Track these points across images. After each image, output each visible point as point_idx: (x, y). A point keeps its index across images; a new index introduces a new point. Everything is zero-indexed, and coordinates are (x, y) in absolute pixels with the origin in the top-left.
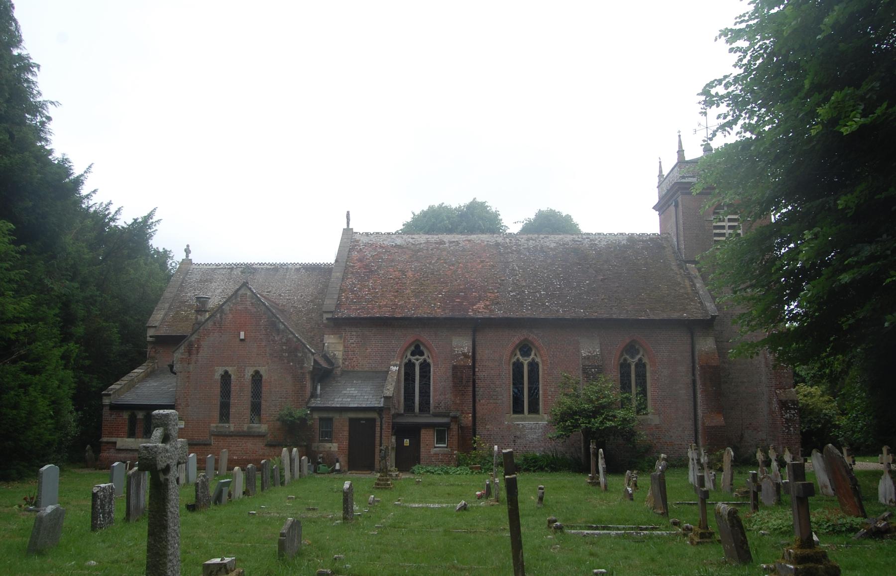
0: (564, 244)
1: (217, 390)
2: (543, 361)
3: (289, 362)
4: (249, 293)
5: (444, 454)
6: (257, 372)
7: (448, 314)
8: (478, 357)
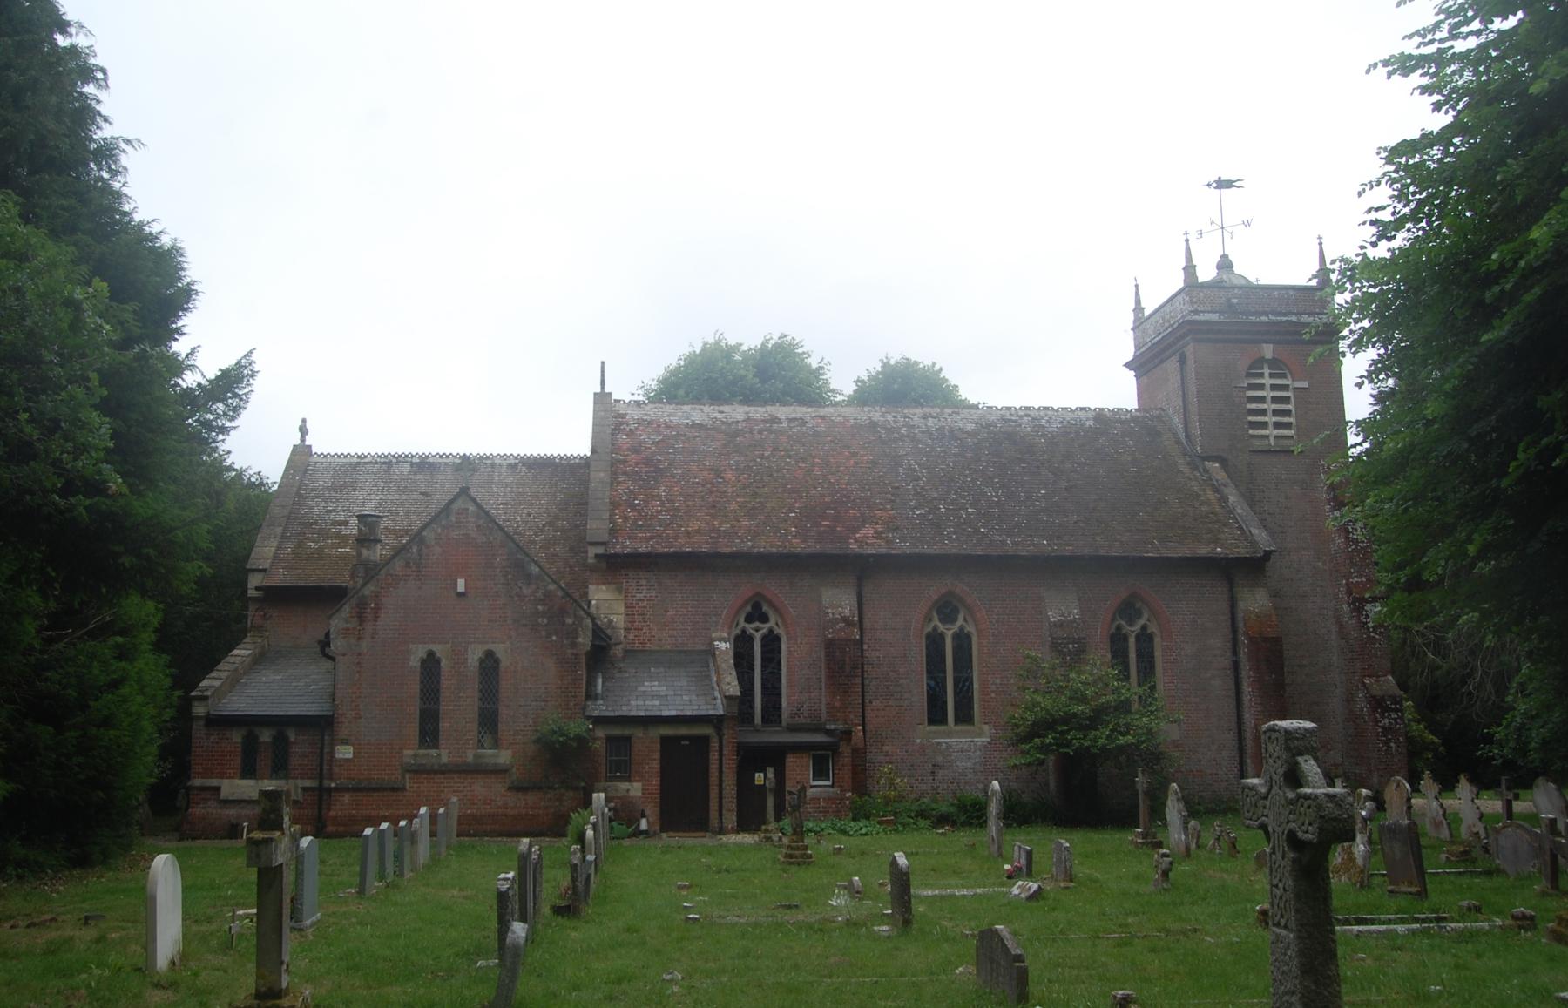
0: (988, 426)
1: (415, 687)
2: (788, 633)
3: (549, 635)
4: (472, 508)
5: (829, 799)
6: (490, 654)
7: (814, 547)
8: (867, 624)
